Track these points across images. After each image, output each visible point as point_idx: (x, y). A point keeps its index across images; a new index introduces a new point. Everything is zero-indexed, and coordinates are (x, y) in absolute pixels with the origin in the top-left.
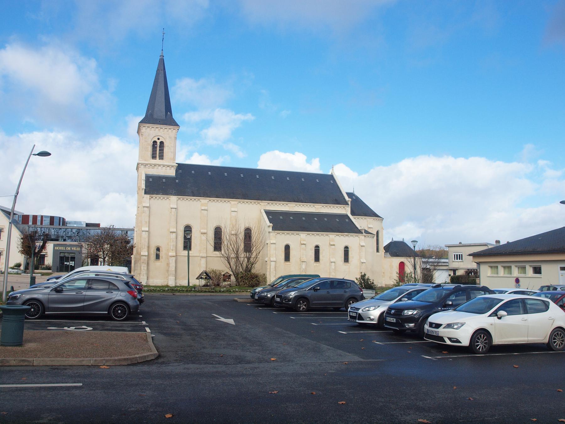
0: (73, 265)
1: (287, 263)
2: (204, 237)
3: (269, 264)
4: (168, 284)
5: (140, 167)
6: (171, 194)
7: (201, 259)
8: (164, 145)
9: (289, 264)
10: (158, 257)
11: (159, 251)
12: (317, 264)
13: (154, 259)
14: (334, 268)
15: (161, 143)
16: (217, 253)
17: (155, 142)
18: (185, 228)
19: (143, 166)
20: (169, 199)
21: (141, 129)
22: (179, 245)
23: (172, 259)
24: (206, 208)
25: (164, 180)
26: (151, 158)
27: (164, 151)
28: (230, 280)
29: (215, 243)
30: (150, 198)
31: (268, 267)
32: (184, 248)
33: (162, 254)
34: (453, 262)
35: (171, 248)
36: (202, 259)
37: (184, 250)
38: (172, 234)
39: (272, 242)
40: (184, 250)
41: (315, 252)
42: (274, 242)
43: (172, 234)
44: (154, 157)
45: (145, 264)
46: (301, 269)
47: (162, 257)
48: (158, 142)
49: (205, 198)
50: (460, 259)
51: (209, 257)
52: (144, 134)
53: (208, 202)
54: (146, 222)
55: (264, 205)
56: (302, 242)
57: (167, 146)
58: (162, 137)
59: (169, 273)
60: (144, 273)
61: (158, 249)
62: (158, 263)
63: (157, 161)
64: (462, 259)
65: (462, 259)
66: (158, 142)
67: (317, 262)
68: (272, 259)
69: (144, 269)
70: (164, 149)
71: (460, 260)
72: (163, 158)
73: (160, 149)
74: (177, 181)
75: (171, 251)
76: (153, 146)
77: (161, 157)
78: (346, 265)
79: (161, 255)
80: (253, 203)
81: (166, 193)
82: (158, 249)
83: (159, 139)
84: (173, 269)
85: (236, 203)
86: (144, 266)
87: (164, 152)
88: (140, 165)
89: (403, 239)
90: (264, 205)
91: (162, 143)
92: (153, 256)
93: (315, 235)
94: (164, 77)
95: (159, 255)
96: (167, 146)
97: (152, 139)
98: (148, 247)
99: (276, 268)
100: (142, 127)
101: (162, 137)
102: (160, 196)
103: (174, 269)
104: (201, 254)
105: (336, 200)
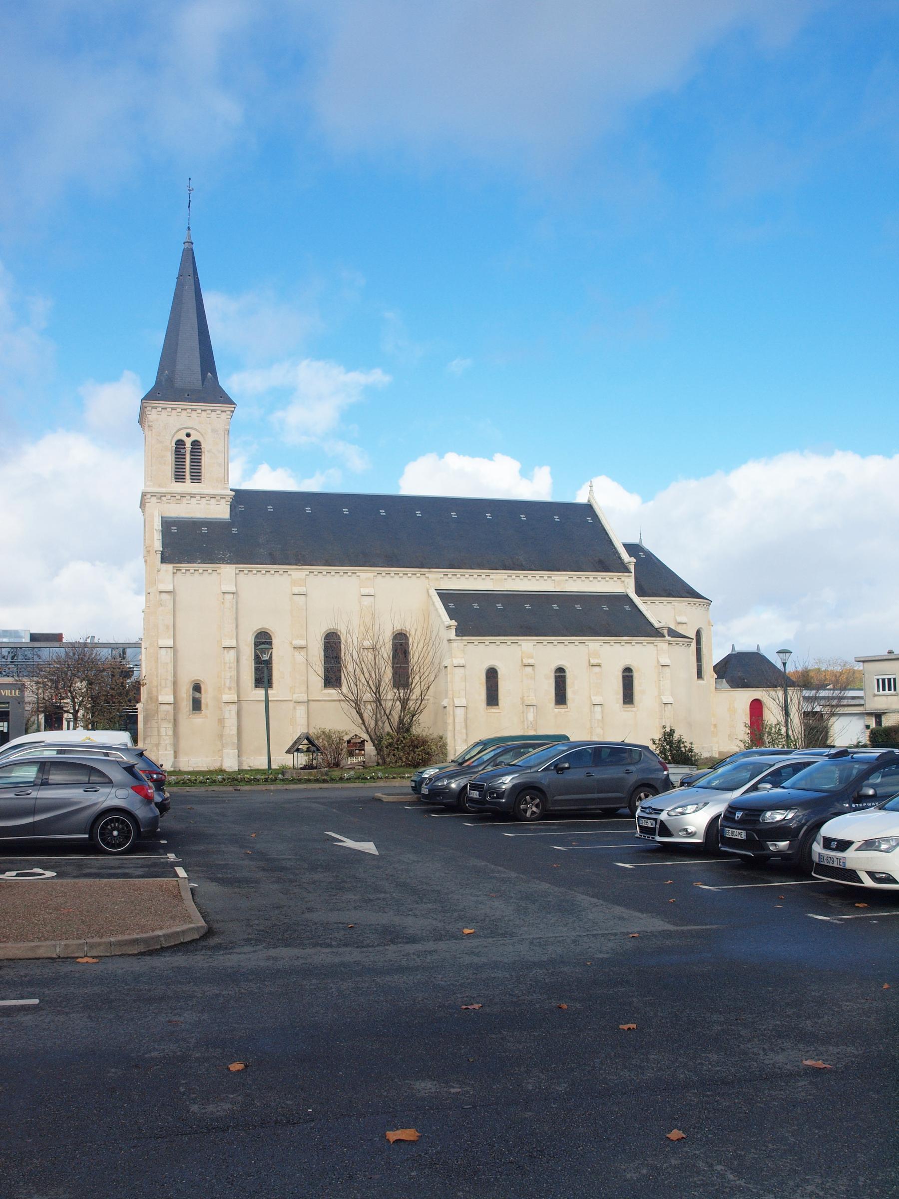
0: (5, 730)
1: (494, 710)
2: (300, 657)
3: (451, 713)
4: (222, 765)
5: (149, 500)
6: (223, 561)
7: (295, 708)
8: (200, 449)
9: (497, 711)
10: (197, 705)
11: (200, 693)
12: (561, 710)
13: (187, 709)
14: (600, 718)
15: (195, 445)
16: (332, 692)
17: (180, 443)
18: (256, 637)
19: (155, 498)
20: (218, 571)
21: (147, 413)
22: (245, 677)
23: (228, 708)
24: (302, 590)
25: (204, 530)
26: (174, 480)
27: (203, 461)
28: (363, 752)
29: (327, 670)
30: (175, 571)
31: (450, 721)
32: (255, 683)
33: (206, 698)
34: (875, 695)
35: (227, 685)
36: (297, 708)
37: (256, 686)
38: (228, 652)
39: (456, 662)
40: (256, 686)
41: (556, 682)
42: (462, 662)
43: (228, 652)
44: (179, 477)
45: (170, 722)
46: (526, 723)
47: (207, 705)
48: (188, 442)
49: (300, 567)
50: (890, 689)
51: (313, 701)
52: (153, 426)
53: (306, 575)
54: (168, 627)
55: (437, 579)
56: (526, 661)
57: (208, 451)
58: (196, 430)
59: (224, 741)
60: (167, 742)
61: (197, 688)
62: (198, 720)
63: (188, 486)
64: (895, 690)
65: (895, 690)
66: (188, 442)
67: (562, 706)
68: (457, 703)
69: (166, 735)
70: (203, 457)
71: (878, 693)
72: (200, 479)
73: (192, 459)
74: (234, 530)
75: (227, 690)
76: (176, 451)
77: (196, 477)
78: (628, 711)
79: (203, 701)
80: (401, 575)
81: (210, 559)
82: (197, 688)
83: (188, 435)
84: (231, 733)
85: (371, 575)
86: (166, 728)
87: (203, 464)
88: (149, 496)
89: (758, 645)
90: (437, 579)
91: (196, 444)
92: (186, 704)
93: (555, 643)
94: (202, 357)
95: (201, 701)
96: (208, 451)
97: (172, 440)
98: (175, 683)
99: (468, 722)
100: (149, 408)
101: (196, 430)
102: (196, 565)
103: (234, 731)
104: (295, 696)
105: (601, 562)
